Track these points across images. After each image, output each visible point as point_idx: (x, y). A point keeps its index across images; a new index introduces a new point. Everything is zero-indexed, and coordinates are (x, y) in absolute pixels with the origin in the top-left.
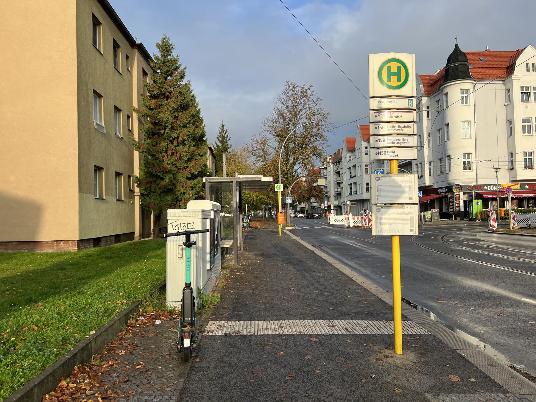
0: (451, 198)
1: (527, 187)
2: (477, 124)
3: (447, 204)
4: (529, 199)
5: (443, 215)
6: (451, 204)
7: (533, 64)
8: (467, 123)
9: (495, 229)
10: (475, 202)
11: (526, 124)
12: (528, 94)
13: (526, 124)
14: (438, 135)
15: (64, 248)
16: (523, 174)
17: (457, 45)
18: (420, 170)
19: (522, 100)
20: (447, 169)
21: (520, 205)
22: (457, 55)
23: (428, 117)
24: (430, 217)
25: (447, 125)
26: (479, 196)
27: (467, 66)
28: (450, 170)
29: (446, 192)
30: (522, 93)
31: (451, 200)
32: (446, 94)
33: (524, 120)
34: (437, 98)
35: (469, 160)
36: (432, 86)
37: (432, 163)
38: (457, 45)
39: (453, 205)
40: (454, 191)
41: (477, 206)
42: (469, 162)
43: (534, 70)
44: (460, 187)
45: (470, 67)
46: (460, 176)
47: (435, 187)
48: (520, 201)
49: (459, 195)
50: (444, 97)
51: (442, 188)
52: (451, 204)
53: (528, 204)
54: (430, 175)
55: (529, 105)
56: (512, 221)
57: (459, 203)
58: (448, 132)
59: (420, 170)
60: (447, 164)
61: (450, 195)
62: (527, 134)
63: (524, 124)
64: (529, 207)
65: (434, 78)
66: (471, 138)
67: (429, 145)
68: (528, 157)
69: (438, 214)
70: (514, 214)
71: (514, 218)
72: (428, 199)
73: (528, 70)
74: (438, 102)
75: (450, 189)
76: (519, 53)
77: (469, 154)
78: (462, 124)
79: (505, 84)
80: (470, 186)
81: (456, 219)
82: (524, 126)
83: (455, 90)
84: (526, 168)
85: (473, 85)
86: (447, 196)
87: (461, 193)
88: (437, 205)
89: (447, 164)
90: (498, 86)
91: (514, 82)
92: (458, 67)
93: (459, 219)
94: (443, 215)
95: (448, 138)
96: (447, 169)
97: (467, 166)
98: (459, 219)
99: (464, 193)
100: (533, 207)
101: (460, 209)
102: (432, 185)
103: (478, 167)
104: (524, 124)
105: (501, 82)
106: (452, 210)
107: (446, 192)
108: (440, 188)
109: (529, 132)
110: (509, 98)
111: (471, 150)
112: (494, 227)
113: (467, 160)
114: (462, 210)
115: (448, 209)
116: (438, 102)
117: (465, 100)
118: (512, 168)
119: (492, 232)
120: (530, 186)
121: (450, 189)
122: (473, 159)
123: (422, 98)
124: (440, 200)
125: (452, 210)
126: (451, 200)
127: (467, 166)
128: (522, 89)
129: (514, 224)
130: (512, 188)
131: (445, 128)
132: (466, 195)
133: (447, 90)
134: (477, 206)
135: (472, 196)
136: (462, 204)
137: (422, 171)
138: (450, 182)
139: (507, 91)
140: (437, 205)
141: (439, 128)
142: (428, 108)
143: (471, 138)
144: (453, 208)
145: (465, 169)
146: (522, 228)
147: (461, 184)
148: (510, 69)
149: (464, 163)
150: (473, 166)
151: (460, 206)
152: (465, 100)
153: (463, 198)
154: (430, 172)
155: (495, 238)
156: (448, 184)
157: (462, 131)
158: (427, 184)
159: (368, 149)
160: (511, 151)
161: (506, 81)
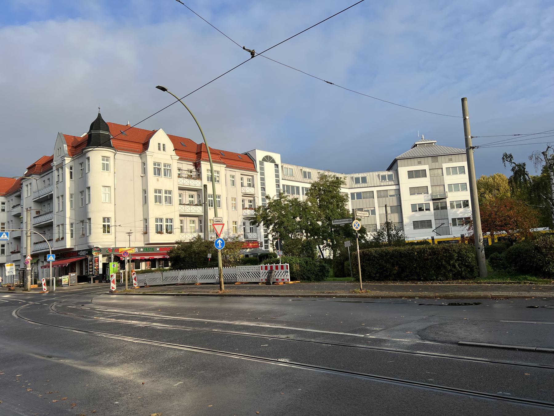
0: (91, 261)
1: (142, 250)
2: (116, 190)
3: (87, 266)
4: (159, 260)
5: (81, 279)
6: (91, 266)
7: (164, 145)
8: (107, 189)
9: (114, 290)
10: (111, 264)
11: (158, 194)
12: (159, 170)
13: (158, 194)
14: (80, 197)
15: (159, 391)
16: (155, 238)
17: (99, 115)
18: (61, 231)
19: (155, 174)
20: (88, 231)
21: (153, 266)
22: (98, 124)
23: (71, 177)
24: (67, 282)
25: (89, 188)
26: (117, 259)
27: (109, 136)
28: (90, 233)
29: (87, 254)
30: (155, 168)
31: (91, 263)
32: (88, 158)
33: (156, 191)
34: (81, 160)
35: (108, 224)
36: (76, 147)
37: (74, 225)
38: (99, 115)
39: (92, 268)
40: (94, 253)
41: (114, 267)
42: (109, 226)
43: (164, 150)
44: (99, 250)
45: (111, 137)
46: (99, 239)
47: (76, 249)
48: (153, 262)
49: (98, 257)
50: (87, 161)
51: (83, 250)
52: (91, 266)
53: (159, 264)
54: (72, 237)
55: (159, 178)
56: (134, 282)
57: (98, 266)
58: (89, 195)
59: (61, 231)
60: (88, 227)
61: (89, 258)
62: (158, 203)
63: (156, 194)
64: (160, 267)
65: (79, 140)
66: (111, 203)
67: (71, 207)
68: (159, 224)
69: (76, 278)
70: (135, 275)
71: (135, 279)
72: (66, 262)
73: (159, 149)
74: (81, 164)
75: (90, 251)
76: (154, 132)
77: (108, 219)
78: (102, 189)
79: (141, 158)
80: (109, 249)
81: (94, 282)
82: (156, 196)
83: (97, 156)
84: (158, 232)
85: (113, 154)
86: (87, 259)
87: (100, 256)
88: (77, 269)
89: (88, 227)
90: (134, 159)
91: (149, 158)
92: (99, 135)
93: (97, 282)
94: (81, 279)
95: (89, 202)
96: (88, 231)
97: (106, 229)
98: (97, 282)
99: (104, 256)
100: (162, 267)
101: (98, 272)
102: (73, 247)
103: (117, 230)
104: (156, 194)
105: (138, 155)
106: (91, 273)
107: (87, 254)
108: (80, 251)
109: (160, 202)
110: (145, 171)
111: (111, 215)
112: (113, 288)
113: (106, 224)
114: (101, 272)
115: (87, 272)
116: (81, 164)
117: (106, 167)
118: (146, 233)
119: (112, 293)
120: (160, 248)
121: (90, 251)
122: (112, 223)
123: (65, 158)
124: (81, 262)
125: (91, 273)
126: (91, 263)
127: (106, 229)
128: (155, 164)
129: (135, 284)
130: (128, 252)
131: (87, 191)
132: (106, 258)
133: (89, 154)
134: (114, 267)
135: (110, 258)
136: (101, 266)
137: (63, 233)
138: (90, 244)
139: (143, 164)
140: (77, 269)
141: (81, 190)
142: (71, 168)
143: (111, 203)
144: (92, 271)
145: (104, 232)
146: (141, 287)
147: (100, 247)
148: (146, 146)
149: (104, 226)
150: (112, 229)
151: (98, 269)
152: (106, 167)
153: (102, 260)
154: (72, 234)
155: (114, 299)
156: (89, 246)
157: (103, 195)
158: (68, 247)
159: (6, 205)
160: (145, 217)
161: (142, 155)
